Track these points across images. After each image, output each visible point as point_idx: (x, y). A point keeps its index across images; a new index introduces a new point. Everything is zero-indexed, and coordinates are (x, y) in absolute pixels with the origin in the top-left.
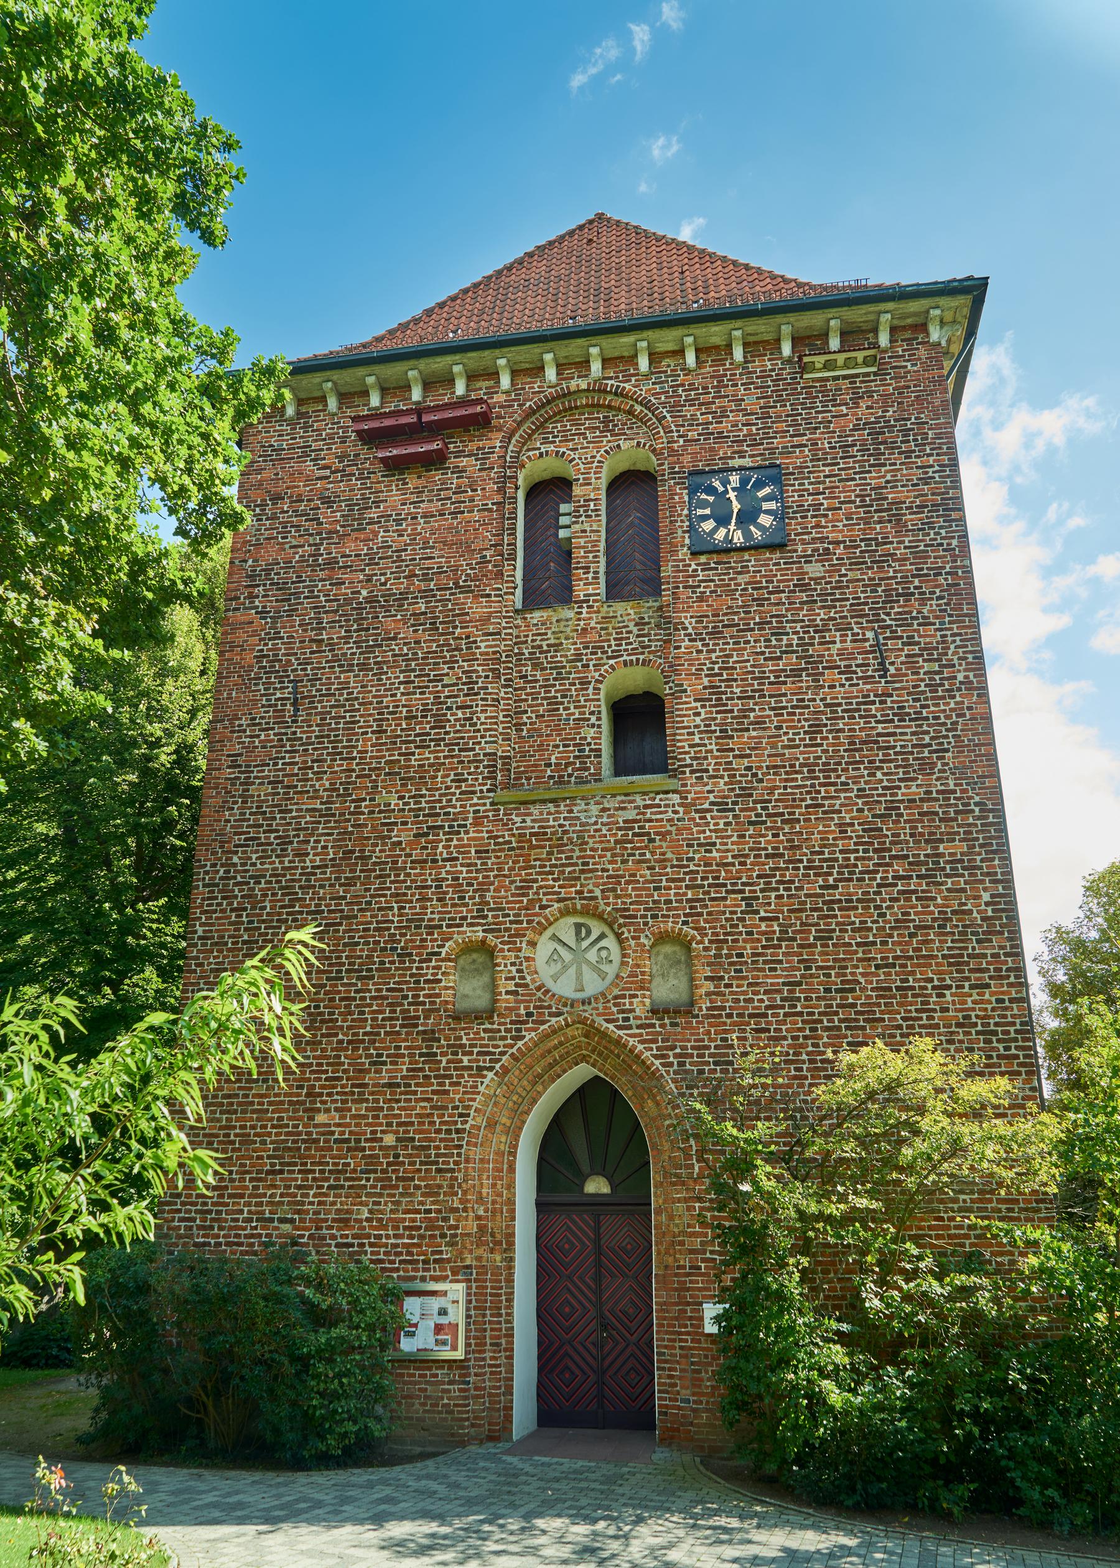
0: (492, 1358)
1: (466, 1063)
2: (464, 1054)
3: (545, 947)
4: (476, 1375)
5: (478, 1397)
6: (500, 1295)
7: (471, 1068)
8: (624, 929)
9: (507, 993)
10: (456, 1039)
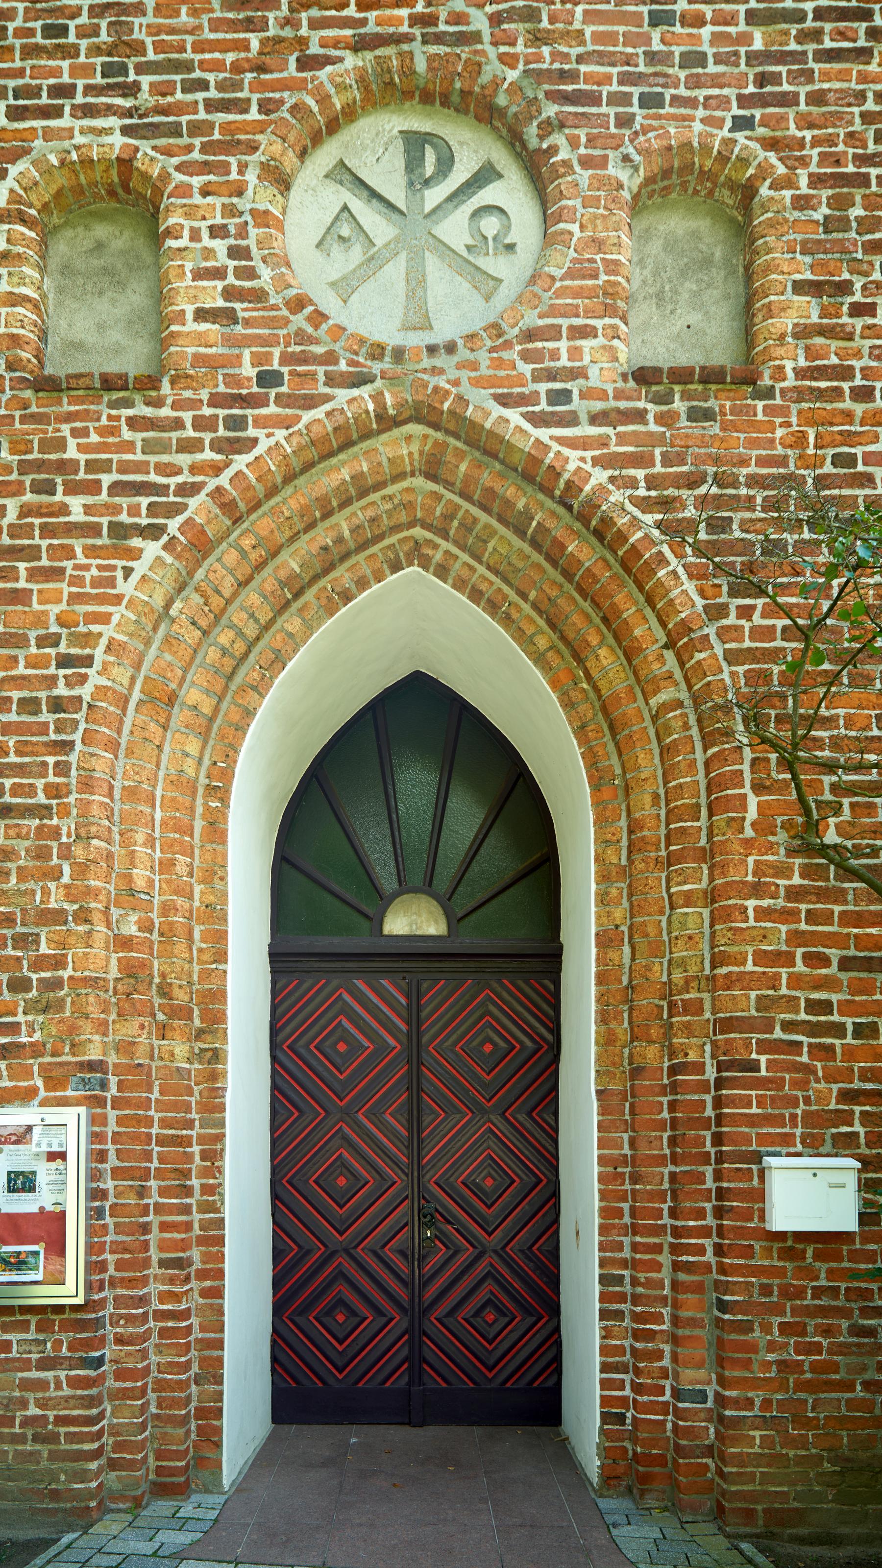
0: (163, 1297)
1: (77, 515)
2: (72, 489)
3: (312, 202)
4: (120, 1340)
5: (125, 1394)
6: (186, 1142)
7: (94, 530)
8: (559, 139)
9: (201, 315)
10: (49, 445)
